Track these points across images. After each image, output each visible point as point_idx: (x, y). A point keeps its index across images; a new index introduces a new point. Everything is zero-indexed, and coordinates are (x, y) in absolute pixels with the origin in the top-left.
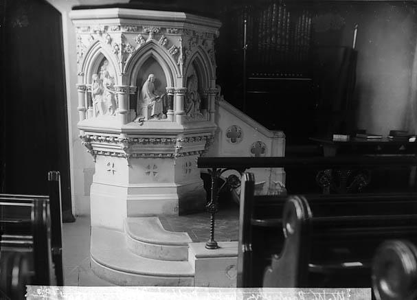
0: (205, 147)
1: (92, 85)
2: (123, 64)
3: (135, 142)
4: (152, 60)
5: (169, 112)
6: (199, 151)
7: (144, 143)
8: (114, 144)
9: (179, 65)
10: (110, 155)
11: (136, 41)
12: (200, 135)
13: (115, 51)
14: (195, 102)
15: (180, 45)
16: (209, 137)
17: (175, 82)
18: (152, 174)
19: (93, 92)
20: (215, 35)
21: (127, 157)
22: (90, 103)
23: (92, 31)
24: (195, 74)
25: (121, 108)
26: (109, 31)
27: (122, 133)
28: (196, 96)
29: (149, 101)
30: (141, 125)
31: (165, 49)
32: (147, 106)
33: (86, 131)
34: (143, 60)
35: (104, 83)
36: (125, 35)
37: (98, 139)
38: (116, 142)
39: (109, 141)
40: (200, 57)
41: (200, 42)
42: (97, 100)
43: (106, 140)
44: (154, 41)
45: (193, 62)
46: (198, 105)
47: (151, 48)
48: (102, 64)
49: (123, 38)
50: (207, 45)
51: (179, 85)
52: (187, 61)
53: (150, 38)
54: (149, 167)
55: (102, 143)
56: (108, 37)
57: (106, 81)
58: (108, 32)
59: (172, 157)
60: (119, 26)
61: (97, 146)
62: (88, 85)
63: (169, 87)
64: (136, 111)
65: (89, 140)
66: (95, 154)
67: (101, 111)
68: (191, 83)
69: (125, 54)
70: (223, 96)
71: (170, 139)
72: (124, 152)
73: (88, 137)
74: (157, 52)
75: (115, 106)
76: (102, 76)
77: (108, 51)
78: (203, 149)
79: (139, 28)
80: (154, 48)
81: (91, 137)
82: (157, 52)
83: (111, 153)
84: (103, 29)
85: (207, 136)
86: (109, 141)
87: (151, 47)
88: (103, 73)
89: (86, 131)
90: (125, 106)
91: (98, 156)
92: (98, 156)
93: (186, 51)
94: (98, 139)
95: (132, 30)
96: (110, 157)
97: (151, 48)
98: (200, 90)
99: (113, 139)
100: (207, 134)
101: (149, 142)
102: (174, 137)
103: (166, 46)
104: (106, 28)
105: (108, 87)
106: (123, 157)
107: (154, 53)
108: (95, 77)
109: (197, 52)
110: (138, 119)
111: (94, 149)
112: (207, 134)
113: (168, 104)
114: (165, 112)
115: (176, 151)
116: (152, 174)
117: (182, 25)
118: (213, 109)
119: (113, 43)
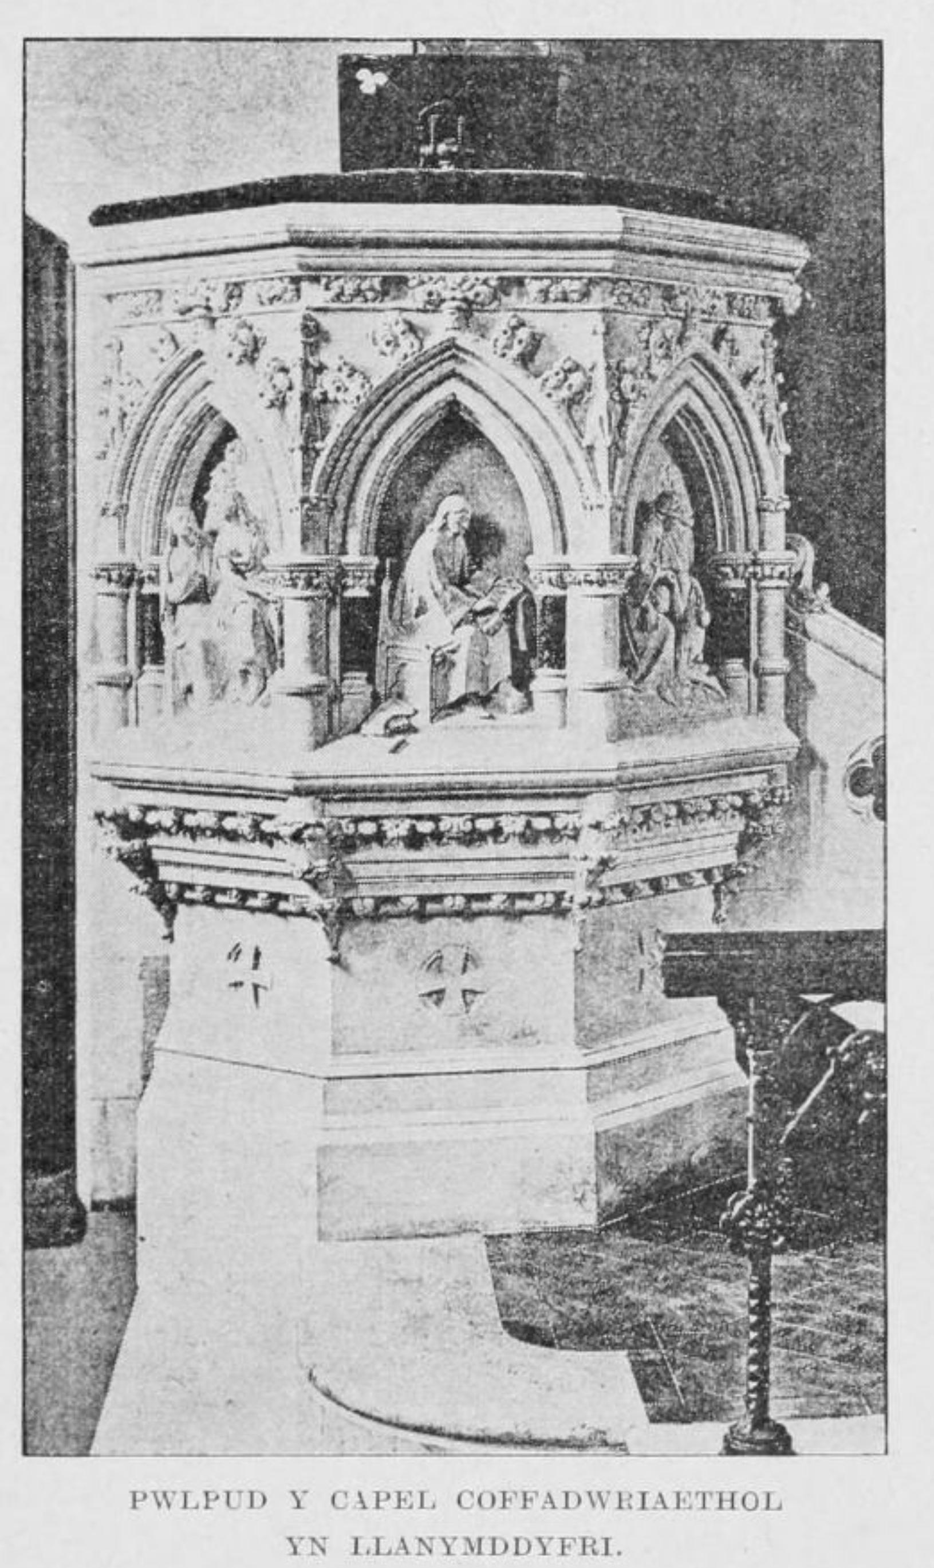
0: (740, 850)
1: (161, 560)
2: (308, 451)
3: (367, 840)
4: (455, 429)
5: (544, 679)
6: (708, 874)
7: (414, 840)
8: (259, 848)
9: (590, 449)
10: (210, 902)
11: (367, 344)
12: (708, 789)
13: (270, 395)
14: (680, 625)
15: (590, 351)
16: (756, 799)
17: (571, 528)
18: (454, 1001)
19: (170, 591)
20: (775, 306)
21: (324, 914)
22: (152, 646)
23: (169, 313)
24: (680, 487)
25: (297, 669)
26: (248, 304)
27: (297, 792)
28: (688, 590)
29: (433, 628)
30: (395, 750)
31: (517, 374)
32: (426, 658)
33: (127, 784)
34: (418, 423)
35: (223, 545)
36: (326, 321)
37: (180, 825)
38: (269, 839)
39: (233, 836)
40: (697, 405)
41: (699, 341)
42: (184, 630)
43: (220, 832)
44: (465, 339)
45: (667, 430)
46: (697, 639)
47: (453, 374)
48: (216, 454)
49: (314, 335)
50: (734, 352)
51: (594, 544)
52: (633, 430)
53: (441, 327)
54: (436, 964)
55: (202, 843)
56: (244, 335)
57: (234, 538)
58: (241, 310)
59: (558, 910)
60: (296, 280)
61: (179, 860)
62: (144, 565)
63: (544, 555)
64: (371, 680)
65: (143, 830)
66: (167, 902)
67: (202, 686)
68: (655, 529)
69: (315, 405)
70: (825, 589)
71: (435, 818)
72: (304, 888)
73: (134, 815)
74: (476, 388)
75: (272, 648)
76: (214, 518)
77: (238, 395)
78: (730, 857)
79: (394, 284)
80: (460, 369)
81: (151, 818)
82: (476, 388)
83: (245, 894)
84: (218, 301)
85: (745, 795)
86: (233, 836)
87: (447, 367)
88: (217, 498)
89: (127, 784)
90: (317, 660)
91: (181, 908)
92: (181, 908)
93: (627, 381)
94: (180, 825)
95: (358, 292)
96: (210, 911)
97: (453, 374)
98: (705, 566)
99: (256, 825)
100: (745, 783)
101: (437, 836)
102: (571, 804)
103: (525, 359)
104: (235, 290)
105: (237, 570)
106: (303, 913)
107: (466, 397)
108: (179, 519)
109: (687, 383)
110: (380, 718)
111: (165, 873)
112: (745, 783)
113: (541, 638)
114: (521, 680)
115: (582, 878)
116: (454, 1001)
117: (605, 260)
118: (776, 660)
119: (265, 356)
